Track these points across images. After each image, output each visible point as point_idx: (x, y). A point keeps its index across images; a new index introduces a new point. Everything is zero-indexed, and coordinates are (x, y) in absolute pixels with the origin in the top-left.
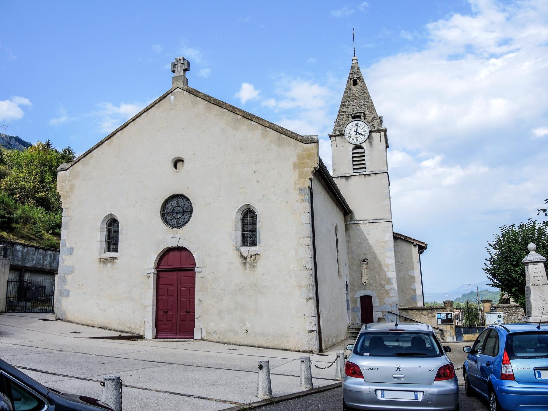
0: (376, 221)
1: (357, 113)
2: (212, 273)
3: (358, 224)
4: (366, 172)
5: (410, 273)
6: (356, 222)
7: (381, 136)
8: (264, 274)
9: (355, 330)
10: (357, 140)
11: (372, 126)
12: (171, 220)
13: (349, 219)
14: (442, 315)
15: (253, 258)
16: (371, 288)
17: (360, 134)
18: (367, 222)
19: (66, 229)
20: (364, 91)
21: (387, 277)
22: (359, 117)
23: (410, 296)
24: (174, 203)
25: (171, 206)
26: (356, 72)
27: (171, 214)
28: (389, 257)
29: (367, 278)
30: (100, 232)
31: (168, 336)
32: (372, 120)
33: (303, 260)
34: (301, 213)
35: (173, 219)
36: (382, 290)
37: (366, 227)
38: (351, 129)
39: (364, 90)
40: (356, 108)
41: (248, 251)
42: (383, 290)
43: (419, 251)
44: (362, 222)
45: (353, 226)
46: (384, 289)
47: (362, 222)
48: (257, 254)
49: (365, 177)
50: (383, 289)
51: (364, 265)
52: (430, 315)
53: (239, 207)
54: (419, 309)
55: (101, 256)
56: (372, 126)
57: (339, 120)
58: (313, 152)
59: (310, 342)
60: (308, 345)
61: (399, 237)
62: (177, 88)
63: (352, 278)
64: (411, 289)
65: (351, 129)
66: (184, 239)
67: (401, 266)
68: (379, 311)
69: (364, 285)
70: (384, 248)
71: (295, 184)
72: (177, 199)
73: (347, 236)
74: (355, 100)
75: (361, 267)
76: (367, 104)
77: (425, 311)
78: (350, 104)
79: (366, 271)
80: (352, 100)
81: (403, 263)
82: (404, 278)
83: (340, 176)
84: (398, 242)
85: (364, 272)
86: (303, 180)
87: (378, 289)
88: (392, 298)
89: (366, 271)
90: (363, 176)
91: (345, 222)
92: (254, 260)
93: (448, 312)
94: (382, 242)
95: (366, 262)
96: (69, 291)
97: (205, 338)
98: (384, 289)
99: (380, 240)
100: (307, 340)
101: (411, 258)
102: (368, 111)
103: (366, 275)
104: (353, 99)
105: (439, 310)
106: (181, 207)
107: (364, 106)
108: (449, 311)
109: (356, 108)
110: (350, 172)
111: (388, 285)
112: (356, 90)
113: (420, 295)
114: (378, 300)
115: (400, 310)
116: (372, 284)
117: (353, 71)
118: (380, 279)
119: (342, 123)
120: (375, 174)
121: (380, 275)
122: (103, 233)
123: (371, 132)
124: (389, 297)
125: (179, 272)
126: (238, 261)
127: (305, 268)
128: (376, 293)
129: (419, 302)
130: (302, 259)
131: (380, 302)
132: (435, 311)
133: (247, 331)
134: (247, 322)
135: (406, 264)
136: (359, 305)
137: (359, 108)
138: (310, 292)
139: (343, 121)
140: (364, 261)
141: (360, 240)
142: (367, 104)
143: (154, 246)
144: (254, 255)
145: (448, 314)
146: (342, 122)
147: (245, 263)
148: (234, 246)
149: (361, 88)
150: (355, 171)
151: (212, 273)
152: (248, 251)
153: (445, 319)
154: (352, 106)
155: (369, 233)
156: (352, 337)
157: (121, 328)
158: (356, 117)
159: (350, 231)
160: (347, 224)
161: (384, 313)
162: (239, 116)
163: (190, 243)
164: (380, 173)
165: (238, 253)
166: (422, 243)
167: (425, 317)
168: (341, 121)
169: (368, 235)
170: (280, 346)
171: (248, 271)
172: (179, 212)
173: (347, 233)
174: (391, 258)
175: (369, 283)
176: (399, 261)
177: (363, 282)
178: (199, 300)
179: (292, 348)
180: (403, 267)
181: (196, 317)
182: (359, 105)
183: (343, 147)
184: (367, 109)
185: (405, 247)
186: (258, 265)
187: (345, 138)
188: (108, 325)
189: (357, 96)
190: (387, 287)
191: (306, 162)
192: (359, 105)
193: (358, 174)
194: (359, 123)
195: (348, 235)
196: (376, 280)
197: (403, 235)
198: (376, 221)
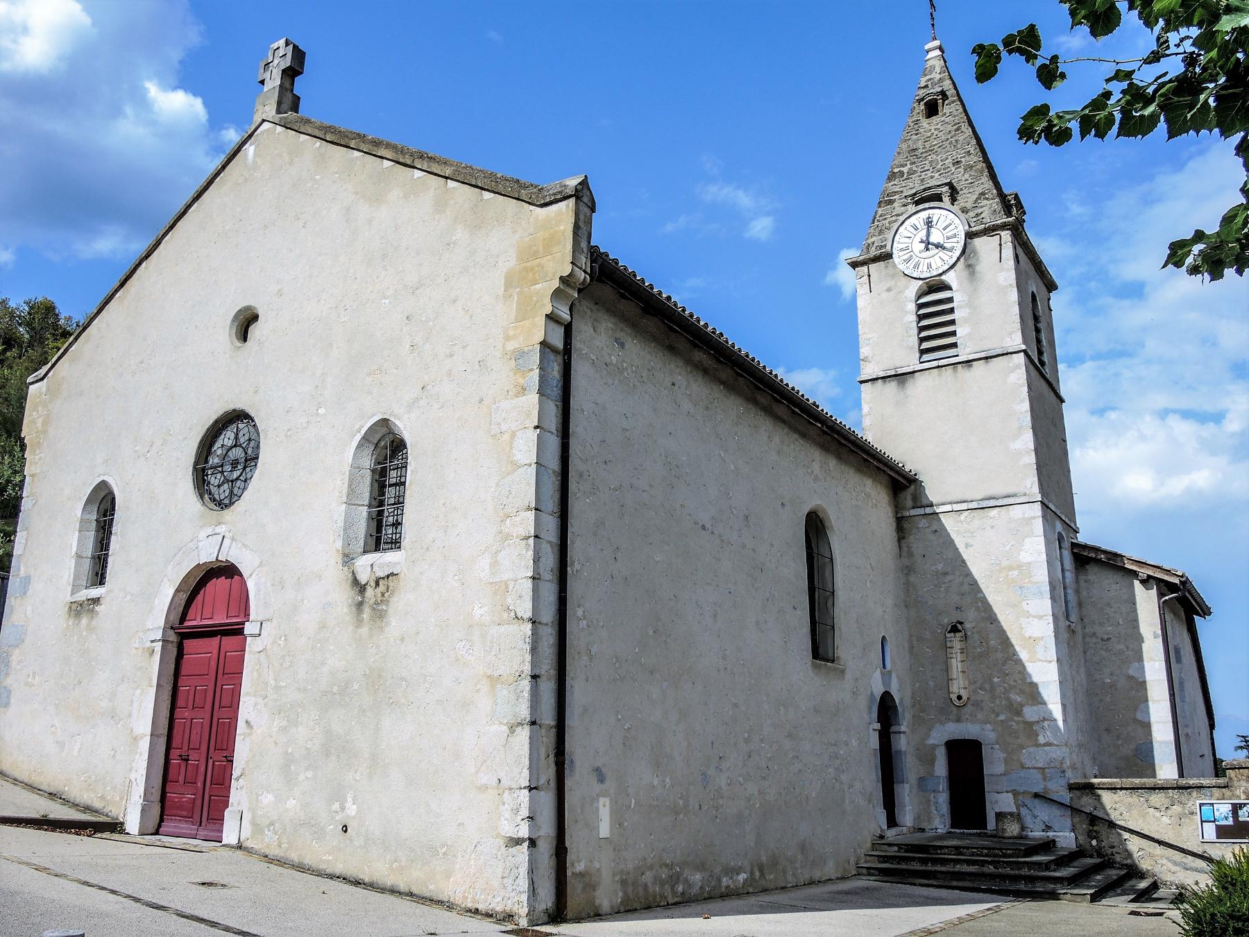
0: (992, 503)
1: (930, 188)
2: (283, 639)
3: (935, 516)
4: (957, 356)
5: (1131, 672)
6: (928, 510)
7: (1001, 245)
8: (402, 639)
9: (896, 848)
10: (929, 266)
11: (975, 219)
12: (219, 486)
13: (909, 503)
14: (1218, 810)
15: (382, 588)
16: (980, 716)
17: (938, 246)
18: (964, 506)
19: (26, 529)
20: (955, 127)
21: (1028, 681)
22: (938, 198)
23: (1132, 747)
24: (227, 438)
25: (222, 446)
26: (936, 80)
27: (220, 469)
28: (1035, 617)
29: (967, 682)
30: (80, 531)
31: (182, 828)
32: (976, 201)
33: (510, 590)
34: (513, 432)
35: (223, 483)
36: (1014, 724)
37: (962, 522)
38: (913, 236)
39: (955, 125)
40: (932, 177)
41: (372, 565)
42: (1018, 723)
43: (1159, 599)
44: (947, 508)
45: (923, 523)
46: (1020, 719)
47: (947, 508)
48: (392, 574)
49: (956, 371)
50: (1016, 718)
51: (956, 642)
52: (1177, 809)
53: (363, 431)
54: (1138, 789)
55: (76, 595)
56: (975, 219)
57: (881, 216)
58: (562, 228)
59: (508, 881)
60: (502, 894)
61: (1090, 555)
62: (264, 121)
63: (918, 685)
64: (1135, 721)
65: (910, 235)
66: (233, 539)
67: (1102, 649)
68: (1005, 789)
69: (955, 708)
70: (1017, 588)
71: (507, 338)
72: (235, 425)
73: (904, 554)
74: (930, 155)
75: (945, 647)
76: (963, 160)
77: (1160, 795)
78: (914, 169)
79: (962, 661)
80: (920, 157)
81: (1109, 639)
82: (1112, 686)
83: (882, 374)
84: (1090, 571)
85: (956, 665)
86: (527, 323)
87: (1002, 717)
88: (1046, 748)
89: (962, 661)
90: (949, 369)
91: (897, 513)
92: (383, 595)
93: (1239, 797)
94: (1011, 568)
95: (960, 631)
96: (10, 692)
97: (248, 844)
98: (1020, 719)
99: (1005, 563)
100: (499, 871)
101: (1134, 622)
102: (964, 179)
103: (960, 674)
104: (924, 155)
105: (1207, 791)
106: (242, 447)
107: (953, 169)
108: (1243, 796)
109: (932, 177)
110: (910, 361)
111: (1032, 705)
112: (933, 128)
113: (1164, 742)
114: (1002, 755)
115: (1073, 789)
116: (982, 701)
117: (929, 80)
118: (1006, 685)
119: (888, 225)
120: (986, 358)
121: (1007, 675)
122: (88, 533)
123: (970, 235)
124: (1038, 745)
125: (223, 637)
126: (343, 597)
127: (513, 614)
128: (993, 733)
129: (1164, 767)
130: (507, 587)
131: (1006, 761)
132: (1194, 794)
133: (345, 829)
134: (349, 799)
135: (1119, 642)
136: (941, 768)
137: (940, 175)
138: (521, 700)
139: (891, 219)
140: (954, 629)
141: (941, 565)
142: (963, 160)
143: (172, 563)
144: (383, 578)
145: (1241, 806)
146: (887, 221)
147: (360, 605)
148: (338, 551)
149: (947, 120)
150: (926, 357)
151: (283, 639)
152: (372, 565)
153: (1230, 822)
154: (919, 174)
155: (970, 541)
156: (877, 873)
157: (87, 798)
158: (927, 198)
159: (911, 539)
160: (903, 517)
161: (1020, 797)
162: (387, 163)
163: (244, 550)
164: (1003, 355)
165: (345, 574)
166: (1168, 572)
167: (1158, 814)
168: (886, 219)
169: (966, 547)
170: (427, 887)
171: (364, 630)
172: (232, 464)
173: (903, 545)
174: (1040, 617)
175: (972, 698)
176: (1094, 634)
177: (954, 697)
178: (247, 722)
179: (457, 899)
180: (1107, 650)
181: (235, 775)
182: (939, 166)
183: (889, 290)
184: (963, 175)
185: (1114, 587)
186: (391, 611)
187: (895, 266)
188: (65, 786)
189: (934, 145)
190: (1030, 713)
191: (539, 265)
192: (939, 166)
193: (935, 364)
194: (936, 213)
195: (905, 549)
196: (993, 689)
197: (1104, 547)
198: (992, 503)
